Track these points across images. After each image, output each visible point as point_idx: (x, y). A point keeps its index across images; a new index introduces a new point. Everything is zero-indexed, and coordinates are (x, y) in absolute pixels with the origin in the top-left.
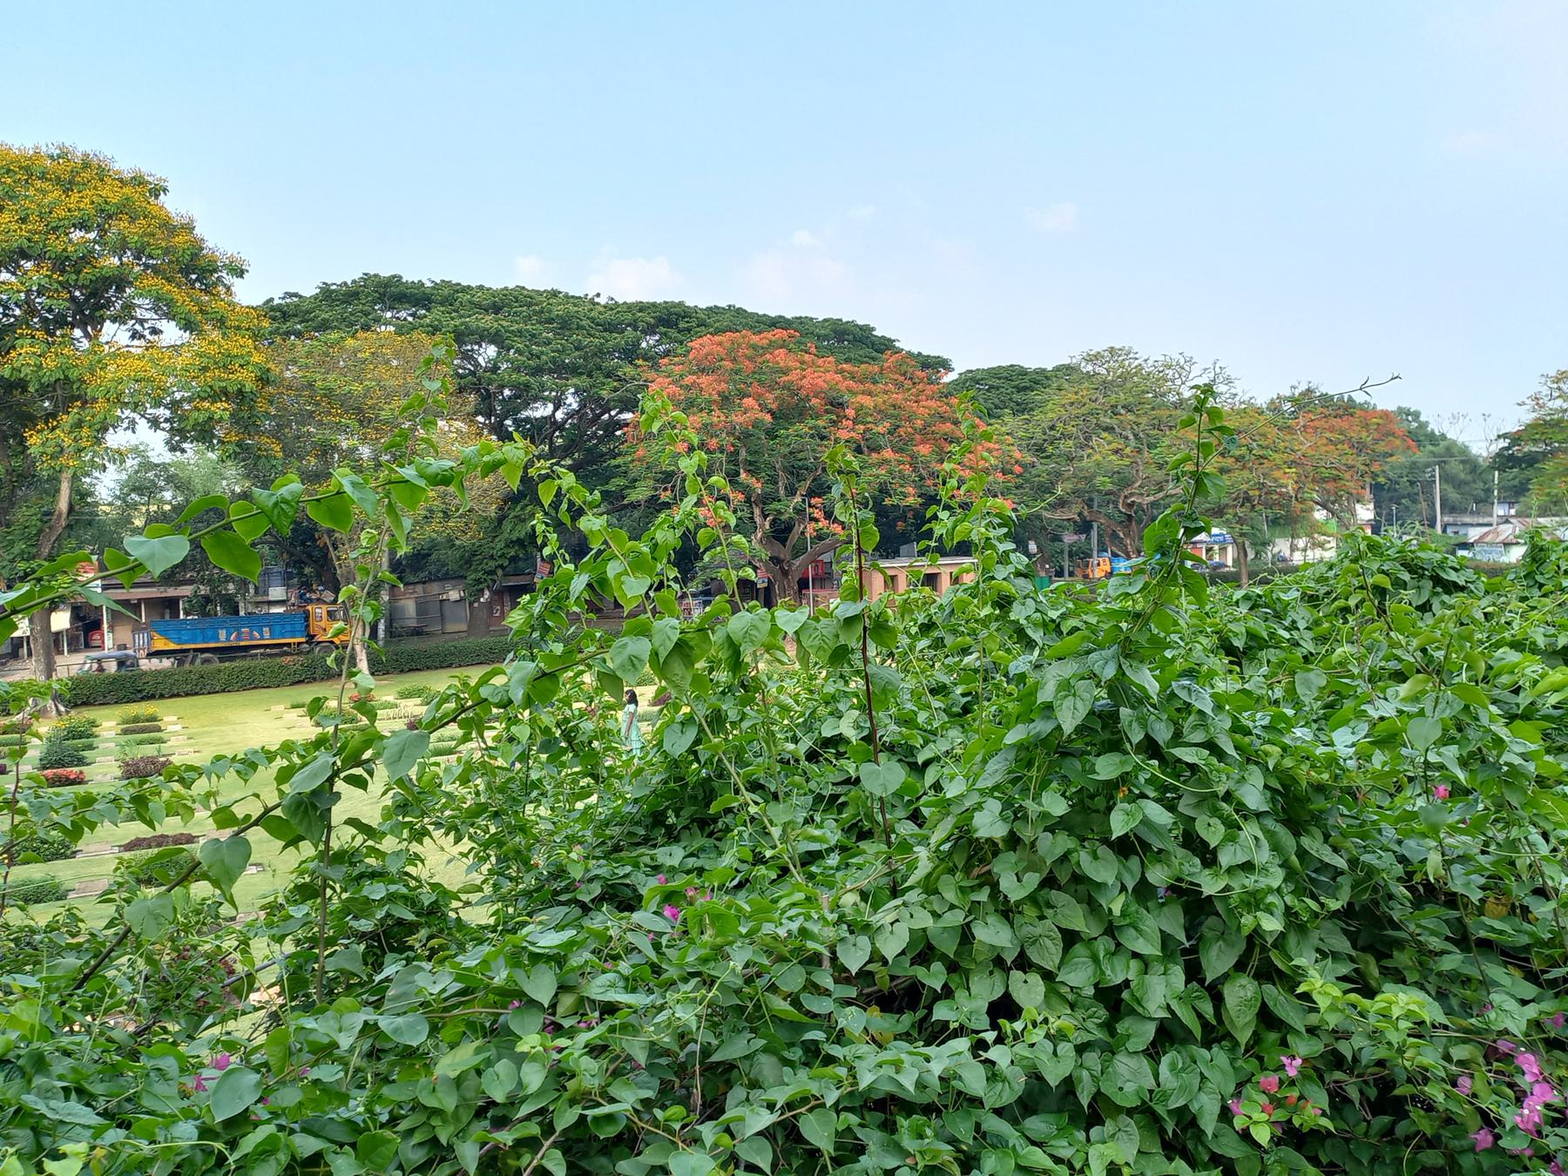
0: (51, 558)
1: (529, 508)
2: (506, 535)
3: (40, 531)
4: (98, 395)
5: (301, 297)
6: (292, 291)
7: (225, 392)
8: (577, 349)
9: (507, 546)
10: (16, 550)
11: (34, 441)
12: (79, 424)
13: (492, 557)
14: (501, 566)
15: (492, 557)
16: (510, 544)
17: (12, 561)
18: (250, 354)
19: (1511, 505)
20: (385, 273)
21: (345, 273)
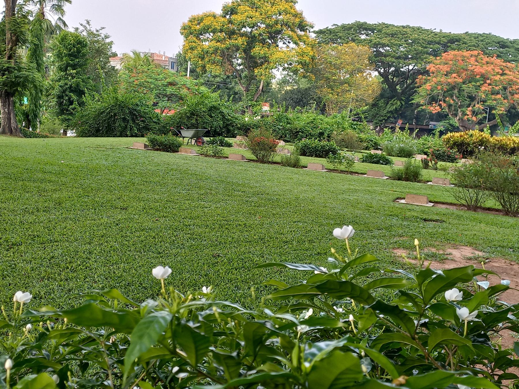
0: (256, 101)
1: (396, 101)
2: (387, 109)
3: (255, 94)
4: (272, 61)
5: (338, 26)
6: (336, 24)
7: (301, 62)
8: (415, 50)
9: (387, 113)
10: (249, 98)
11: (256, 71)
12: (266, 68)
13: (382, 116)
14: (384, 119)
15: (382, 116)
16: (388, 112)
17: (247, 101)
18: (309, 52)
19: (423, 110)
20: (362, 21)
21: (350, 21)
